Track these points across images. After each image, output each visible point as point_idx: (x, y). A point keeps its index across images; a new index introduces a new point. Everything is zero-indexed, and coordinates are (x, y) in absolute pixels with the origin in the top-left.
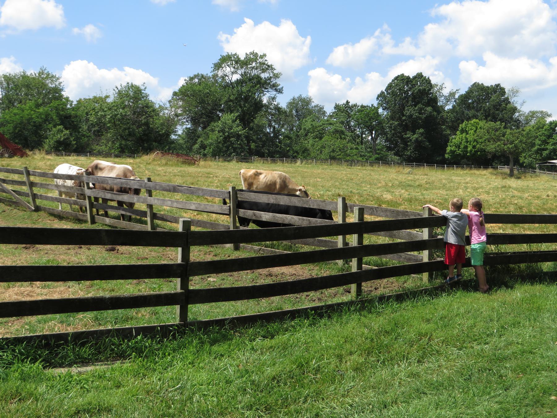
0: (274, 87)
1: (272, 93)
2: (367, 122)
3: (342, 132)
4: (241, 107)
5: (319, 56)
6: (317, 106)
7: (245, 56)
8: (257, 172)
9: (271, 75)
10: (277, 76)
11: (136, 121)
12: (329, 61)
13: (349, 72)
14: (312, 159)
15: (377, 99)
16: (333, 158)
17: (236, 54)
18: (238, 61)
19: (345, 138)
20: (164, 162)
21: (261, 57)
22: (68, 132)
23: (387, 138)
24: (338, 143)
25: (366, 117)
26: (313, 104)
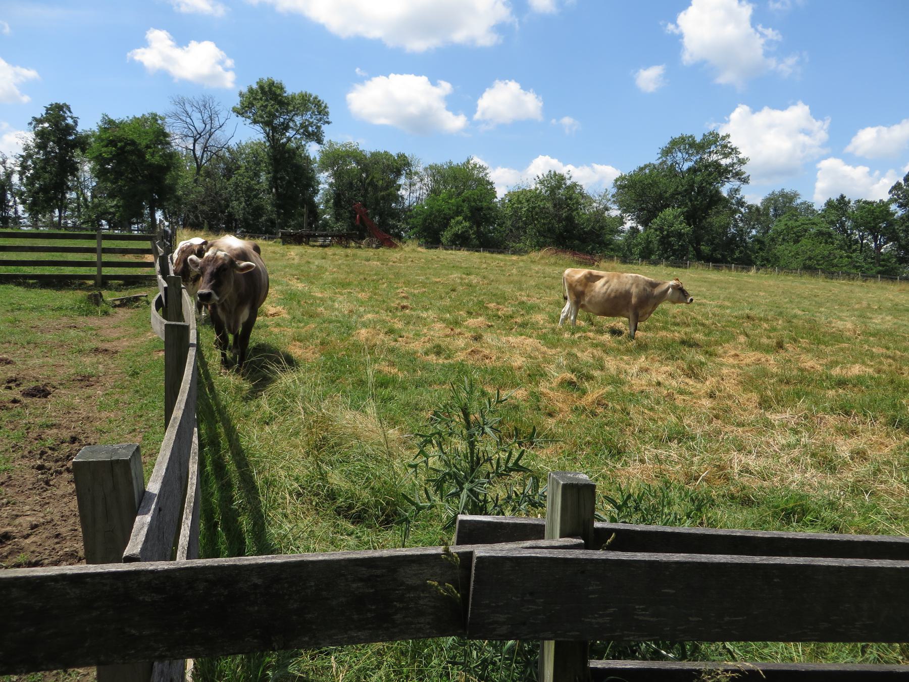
0: (738, 175)
1: (734, 183)
2: (870, 223)
3: (830, 235)
4: (691, 201)
5: (837, 143)
6: (804, 203)
7: (701, 137)
8: (590, 274)
9: (735, 161)
10: (742, 162)
11: (556, 215)
12: (850, 148)
13: (876, 163)
14: (781, 269)
15: (890, 192)
16: (810, 269)
17: (691, 136)
18: (693, 144)
19: (833, 243)
20: (553, 260)
21: (723, 138)
22: (467, 224)
23: (900, 245)
24: (822, 249)
25: (873, 216)
26: (799, 201)
